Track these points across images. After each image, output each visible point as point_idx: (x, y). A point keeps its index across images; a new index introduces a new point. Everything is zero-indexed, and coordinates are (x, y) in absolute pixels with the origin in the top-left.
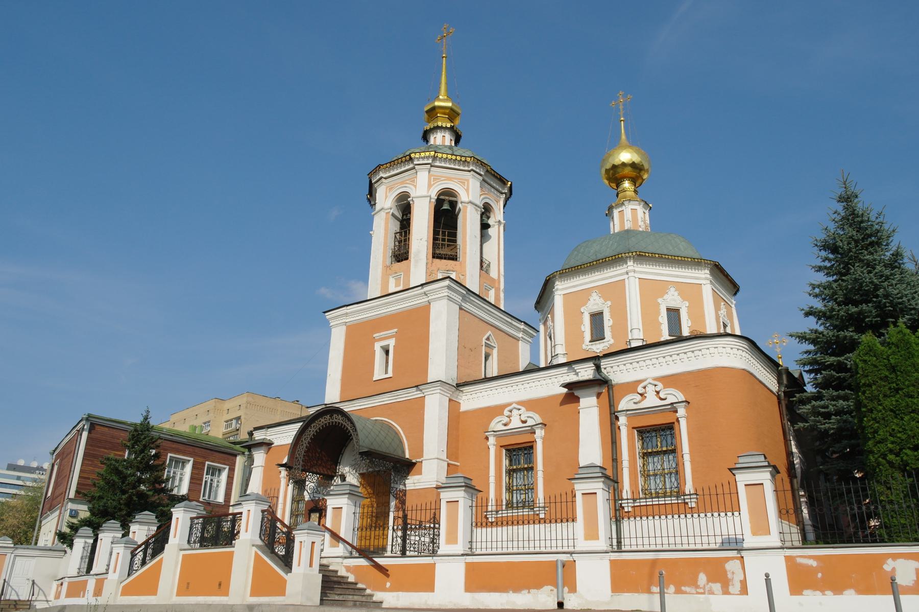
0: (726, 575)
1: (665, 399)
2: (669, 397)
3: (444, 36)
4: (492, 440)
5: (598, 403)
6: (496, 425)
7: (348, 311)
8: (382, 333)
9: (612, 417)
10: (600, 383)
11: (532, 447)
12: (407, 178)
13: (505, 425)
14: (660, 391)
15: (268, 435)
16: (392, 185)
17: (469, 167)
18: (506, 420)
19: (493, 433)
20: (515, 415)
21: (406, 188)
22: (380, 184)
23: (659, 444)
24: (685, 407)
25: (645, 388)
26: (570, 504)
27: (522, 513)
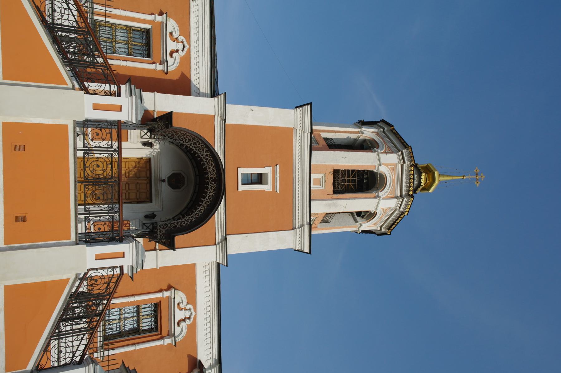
3: (477, 177)
4: (159, 19)
6: (172, 25)
7: (306, 134)
8: (278, 175)
11: (149, 56)
12: (396, 186)
13: (179, 304)
14: (178, 53)
17: (384, 228)
18: (175, 35)
19: (173, 297)
20: (178, 46)
21: (384, 193)
22: (399, 157)
23: (138, 42)
24: (163, 71)
25: (182, 42)
27: (99, 335)
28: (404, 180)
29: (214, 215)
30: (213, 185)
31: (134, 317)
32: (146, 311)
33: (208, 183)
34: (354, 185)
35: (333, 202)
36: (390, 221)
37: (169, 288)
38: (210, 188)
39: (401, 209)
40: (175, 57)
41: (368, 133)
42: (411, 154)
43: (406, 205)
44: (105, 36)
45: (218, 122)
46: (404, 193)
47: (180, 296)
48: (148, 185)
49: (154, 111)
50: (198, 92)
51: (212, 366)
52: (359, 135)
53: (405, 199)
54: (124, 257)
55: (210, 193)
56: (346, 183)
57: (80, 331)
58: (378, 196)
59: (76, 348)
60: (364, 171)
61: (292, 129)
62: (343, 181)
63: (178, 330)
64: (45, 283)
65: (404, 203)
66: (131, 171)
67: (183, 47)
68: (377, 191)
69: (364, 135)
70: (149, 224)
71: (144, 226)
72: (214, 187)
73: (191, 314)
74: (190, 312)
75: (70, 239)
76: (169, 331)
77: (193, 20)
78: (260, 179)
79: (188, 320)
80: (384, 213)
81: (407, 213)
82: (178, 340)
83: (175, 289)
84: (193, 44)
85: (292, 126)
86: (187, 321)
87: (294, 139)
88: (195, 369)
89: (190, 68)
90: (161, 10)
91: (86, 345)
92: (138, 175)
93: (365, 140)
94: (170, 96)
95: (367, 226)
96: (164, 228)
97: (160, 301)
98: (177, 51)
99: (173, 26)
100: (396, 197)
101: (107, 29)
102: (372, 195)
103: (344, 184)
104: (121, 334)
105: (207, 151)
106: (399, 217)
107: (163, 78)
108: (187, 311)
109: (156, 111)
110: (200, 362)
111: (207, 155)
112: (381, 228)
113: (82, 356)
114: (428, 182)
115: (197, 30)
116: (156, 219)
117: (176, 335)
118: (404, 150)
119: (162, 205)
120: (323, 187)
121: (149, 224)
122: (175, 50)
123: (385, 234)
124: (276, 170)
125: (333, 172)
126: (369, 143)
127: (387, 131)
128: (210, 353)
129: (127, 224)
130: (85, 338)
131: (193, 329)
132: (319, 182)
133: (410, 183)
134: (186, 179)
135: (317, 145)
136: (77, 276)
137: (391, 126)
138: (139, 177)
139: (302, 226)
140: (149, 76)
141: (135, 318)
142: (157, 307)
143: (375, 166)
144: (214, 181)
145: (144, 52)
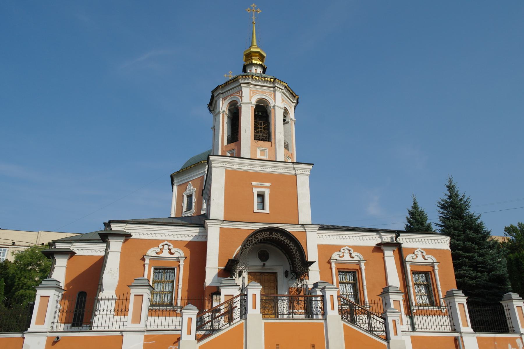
0: (517, 345)
1: (427, 260)
2: (429, 259)
3: (253, 11)
4: (147, 262)
5: (123, 248)
6: (151, 252)
7: (230, 160)
8: (259, 183)
9: (402, 263)
10: (397, 246)
13: (340, 257)
15: (125, 228)
16: (255, 91)
17: (294, 101)
18: (158, 250)
19: (335, 260)
20: (166, 249)
22: (245, 86)
28: (262, 84)
29: (289, 232)
30: (274, 235)
31: (345, 286)
32: (342, 278)
33: (273, 238)
35: (278, 143)
36: (289, 96)
37: (329, 262)
38: (276, 237)
39: (283, 88)
40: (174, 251)
41: (223, 106)
42: (243, 77)
43: (280, 84)
45: (225, 225)
47: (335, 256)
49: (218, 268)
51: (380, 237)
52: (225, 114)
53: (276, 85)
54: (333, 295)
55: (279, 237)
56: (262, 131)
57: (369, 319)
58: (274, 106)
59: (377, 321)
61: (226, 170)
62: (261, 132)
63: (356, 258)
64: (345, 336)
65: (279, 86)
67: (167, 245)
68: (269, 107)
69: (225, 111)
70: (292, 275)
71: (293, 278)
72: (275, 233)
73: (347, 249)
75: (323, 323)
76: (356, 264)
78: (261, 196)
79: (351, 251)
80: (284, 101)
81: (286, 84)
82: (362, 259)
83: (330, 259)
84: (164, 238)
86: (351, 252)
87: (234, 169)
88: (381, 248)
89: (181, 241)
90: (140, 259)
91: (376, 316)
92: (259, 281)
93: (229, 110)
94: (208, 257)
95: (292, 115)
97: (338, 269)
98: (170, 250)
99: (152, 251)
100: (274, 92)
102: (272, 111)
104: (356, 295)
105: (252, 237)
106: (288, 89)
107: (189, 260)
109: (218, 267)
110: (377, 245)
111: (255, 237)
112: (293, 103)
113: (382, 319)
114: (258, 57)
116: (289, 270)
118: (240, 82)
119: (279, 266)
121: (292, 275)
122: (169, 251)
125: (256, 141)
126: (232, 107)
127: (222, 91)
128: (372, 237)
129: (291, 289)
130: (372, 317)
131: (357, 249)
132: (263, 153)
134: (263, 249)
135: (235, 150)
137: (219, 86)
138: (260, 280)
139: (294, 168)
140: (188, 270)
141: (347, 285)
142: (340, 271)
143: (252, 106)
144: (271, 233)
145: (160, 272)
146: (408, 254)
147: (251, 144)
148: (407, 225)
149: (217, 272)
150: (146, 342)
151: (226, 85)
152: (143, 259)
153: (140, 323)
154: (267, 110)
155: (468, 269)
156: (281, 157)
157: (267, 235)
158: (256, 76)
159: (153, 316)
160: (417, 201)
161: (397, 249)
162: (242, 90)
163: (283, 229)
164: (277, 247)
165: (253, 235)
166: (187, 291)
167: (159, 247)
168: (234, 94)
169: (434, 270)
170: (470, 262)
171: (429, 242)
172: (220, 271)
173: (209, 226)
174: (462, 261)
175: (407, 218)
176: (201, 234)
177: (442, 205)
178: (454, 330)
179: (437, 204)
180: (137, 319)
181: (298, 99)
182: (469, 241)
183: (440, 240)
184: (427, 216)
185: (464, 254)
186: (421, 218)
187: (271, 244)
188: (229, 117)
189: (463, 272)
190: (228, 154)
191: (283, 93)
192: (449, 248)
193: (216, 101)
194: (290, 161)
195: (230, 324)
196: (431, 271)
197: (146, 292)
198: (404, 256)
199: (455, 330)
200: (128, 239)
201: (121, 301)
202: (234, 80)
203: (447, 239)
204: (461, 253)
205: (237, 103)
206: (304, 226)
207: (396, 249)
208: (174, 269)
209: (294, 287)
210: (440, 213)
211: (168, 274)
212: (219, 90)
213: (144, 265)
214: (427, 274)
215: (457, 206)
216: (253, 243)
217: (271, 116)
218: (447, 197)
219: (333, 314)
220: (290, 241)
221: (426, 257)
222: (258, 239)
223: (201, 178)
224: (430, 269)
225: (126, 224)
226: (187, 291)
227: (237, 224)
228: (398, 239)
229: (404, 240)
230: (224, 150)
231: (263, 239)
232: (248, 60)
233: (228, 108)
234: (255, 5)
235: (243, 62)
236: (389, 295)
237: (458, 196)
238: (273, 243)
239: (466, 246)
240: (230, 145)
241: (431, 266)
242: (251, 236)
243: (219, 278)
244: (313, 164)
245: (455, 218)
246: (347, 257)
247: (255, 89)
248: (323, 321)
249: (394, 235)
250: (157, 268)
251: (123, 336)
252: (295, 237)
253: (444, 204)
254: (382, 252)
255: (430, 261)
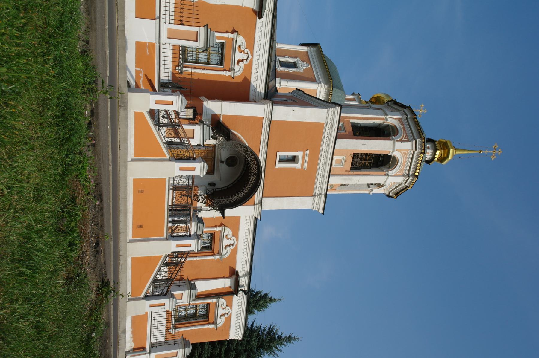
3: (494, 152)
4: (231, 36)
5: (247, 8)
6: (241, 40)
7: (334, 129)
9: (218, 295)
10: (235, 290)
12: (405, 166)
13: (227, 235)
15: (268, 11)
18: (242, 48)
19: (223, 231)
20: (244, 56)
22: (413, 145)
26: (192, 24)
28: (413, 163)
29: (254, 195)
33: (250, 176)
34: (370, 163)
38: (251, 179)
40: (240, 66)
43: (411, 182)
44: (191, 58)
45: (265, 123)
46: (411, 173)
47: (228, 231)
48: (213, 163)
49: (221, 115)
50: (255, 95)
52: (384, 121)
53: (411, 178)
54: (191, 246)
58: (388, 175)
60: (380, 154)
61: (324, 123)
62: (361, 160)
63: (224, 251)
65: (409, 180)
66: (203, 153)
70: (211, 190)
73: (234, 242)
74: (233, 242)
75: (163, 236)
76: (219, 251)
77: (257, 34)
78: (293, 159)
81: (410, 188)
82: (224, 257)
83: (225, 226)
84: (255, 54)
85: (324, 122)
87: (324, 132)
89: (251, 73)
92: (206, 156)
93: (388, 126)
95: (376, 191)
96: (218, 203)
97: (215, 233)
98: (242, 61)
100: (403, 175)
101: (194, 53)
102: (383, 173)
103: (361, 163)
105: (252, 155)
108: (232, 241)
109: (222, 115)
110: (237, 272)
111: (252, 158)
112: (389, 193)
114: (442, 156)
115: (260, 43)
116: (216, 187)
117: (223, 254)
118: (418, 140)
120: (342, 165)
121: (211, 190)
123: (392, 197)
124: (306, 153)
126: (391, 129)
127: (410, 118)
131: (234, 252)
132: (338, 161)
133: (418, 166)
135: (344, 132)
136: (166, 255)
137: (415, 115)
138: (207, 157)
139: (320, 194)
143: (390, 151)
144: (255, 174)
145: (219, 57)
146: (226, 301)
147: (350, 150)
148: (253, 291)
149: (217, 114)
150: (147, 44)
151: (416, 124)
152: (233, 32)
153: (168, 38)
154: (384, 166)
155: (209, 352)
156: (334, 180)
157: (254, 170)
158: (422, 157)
159: (175, 14)
160: (277, 302)
161: (232, 290)
162: (409, 141)
163: (260, 184)
164: (240, 175)
165: (255, 156)
166: (198, 78)
167: (246, 49)
168: (405, 132)
169: (209, 324)
170: (215, 354)
171: (237, 320)
172: (218, 117)
173: (266, 105)
174: (217, 347)
175: (261, 292)
176: (257, 93)
177: (272, 329)
178: (152, 346)
179: (273, 324)
180: (172, 35)
181: (393, 197)
182: (236, 355)
183: (239, 331)
184: (262, 311)
185: (224, 349)
186: (260, 305)
187: (243, 170)
188: (380, 125)
189: (206, 348)
190: (341, 124)
191: (401, 184)
192: (230, 338)
193: (399, 111)
194: (329, 188)
195: (164, 143)
196: (209, 321)
197: (201, 44)
198: (225, 297)
199: (153, 347)
200: (256, 15)
201: (192, 8)
202: (421, 134)
203: (239, 337)
204: (225, 347)
205: (394, 135)
206: (260, 203)
207: (232, 289)
208: (221, 64)
209: (199, 192)
210: (264, 328)
211: (217, 58)
212: (411, 116)
213: (227, 32)
214: (206, 316)
215: (271, 344)
216: (246, 155)
217: (378, 171)
218: (280, 334)
219: (173, 246)
220: (246, 193)
221: (222, 317)
222: (250, 161)
223: (314, 79)
224: (211, 320)
225: (272, 12)
226: (198, 78)
227: (267, 131)
228: (241, 292)
229: (241, 298)
230: (345, 119)
231: (250, 166)
232: (440, 145)
233: (390, 124)
234: (501, 154)
235: (437, 138)
236: (188, 290)
237: (281, 345)
238: (244, 171)
239: (232, 351)
240: (350, 126)
241: (213, 321)
242: (254, 154)
243: (211, 115)
244: (323, 214)
245: (258, 342)
246: (226, 242)
247: (408, 155)
248: (165, 236)
249: (246, 288)
250: (224, 46)
251: (155, 19)
252: (250, 198)
253: (273, 331)
254: (230, 276)
255: (219, 320)
